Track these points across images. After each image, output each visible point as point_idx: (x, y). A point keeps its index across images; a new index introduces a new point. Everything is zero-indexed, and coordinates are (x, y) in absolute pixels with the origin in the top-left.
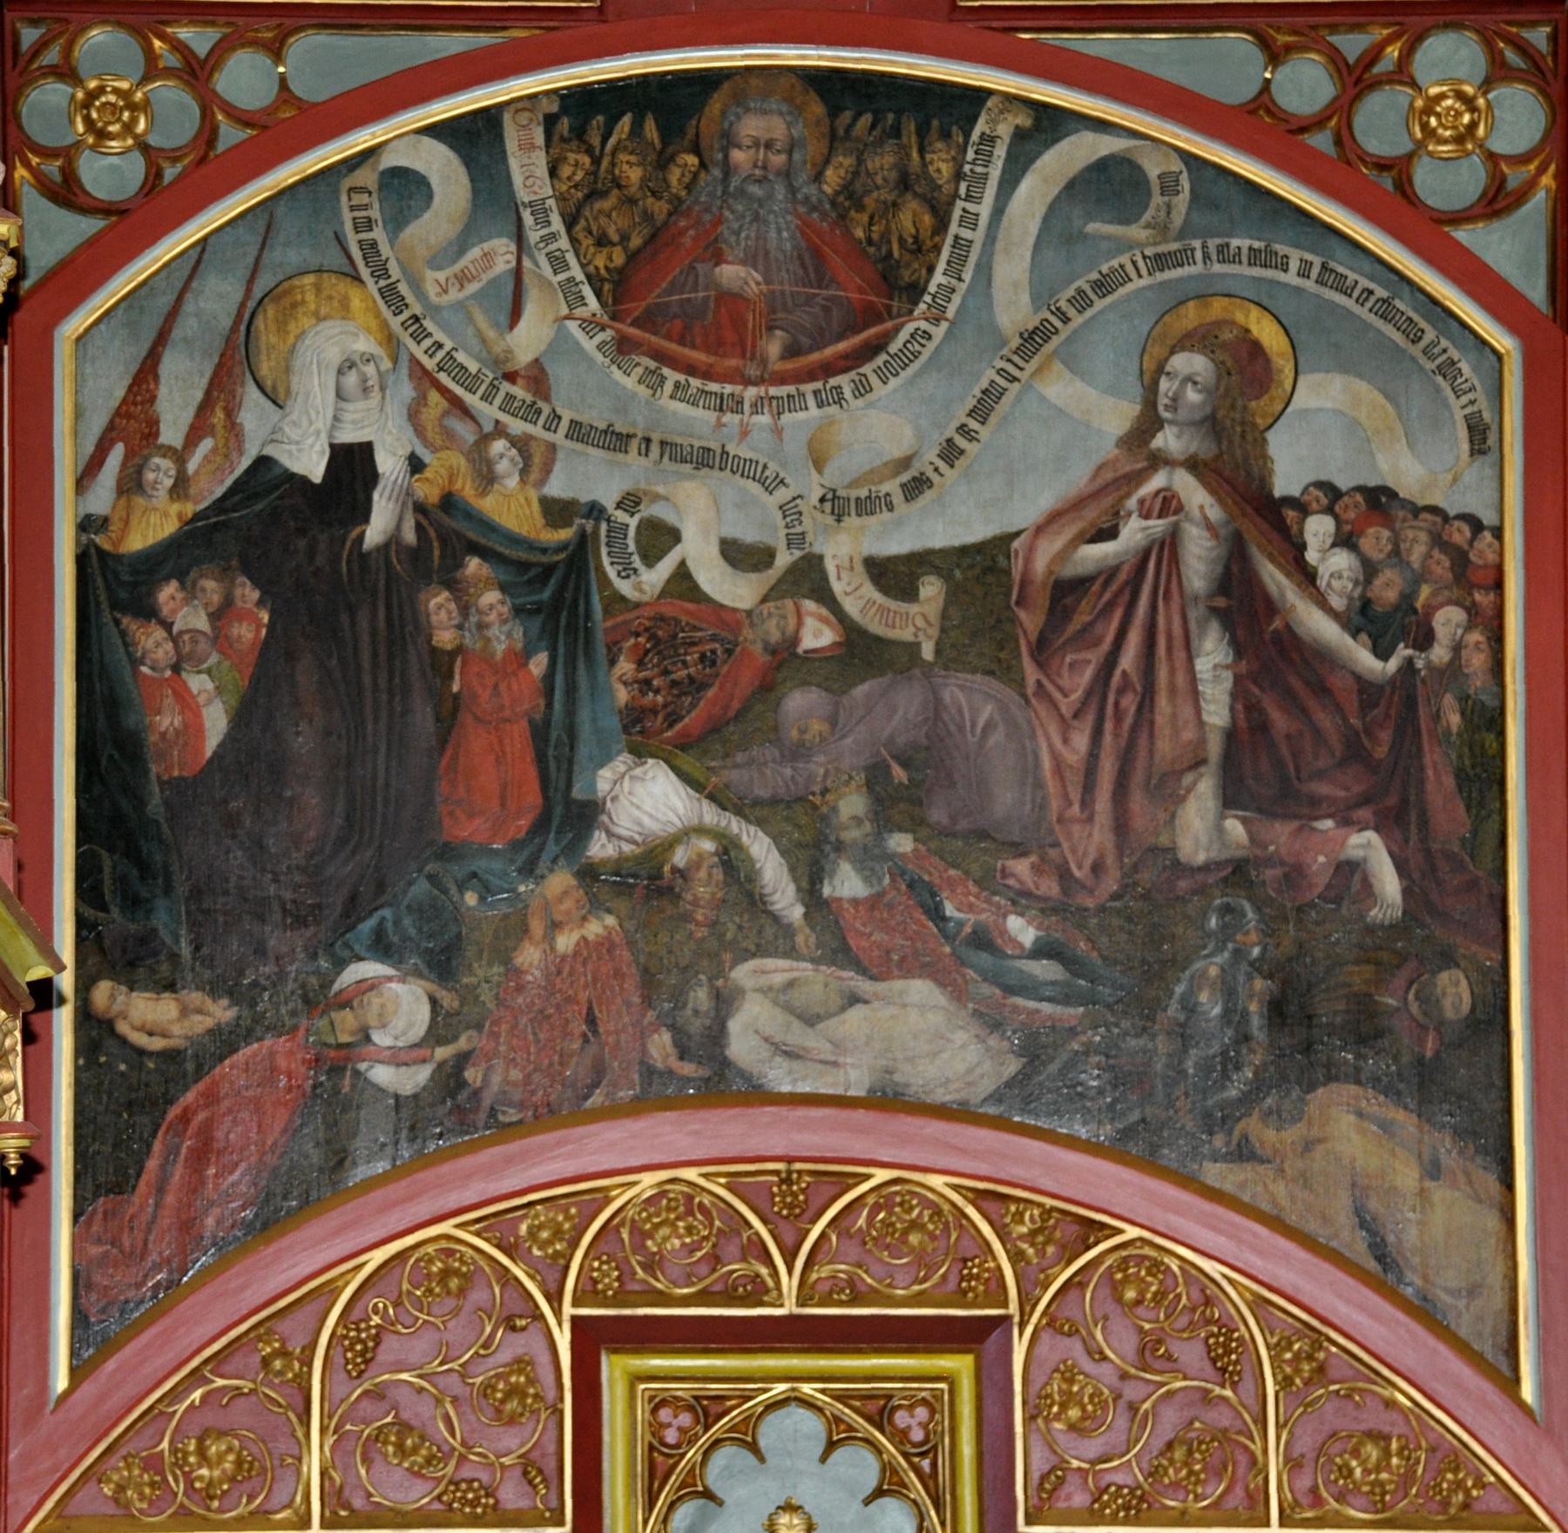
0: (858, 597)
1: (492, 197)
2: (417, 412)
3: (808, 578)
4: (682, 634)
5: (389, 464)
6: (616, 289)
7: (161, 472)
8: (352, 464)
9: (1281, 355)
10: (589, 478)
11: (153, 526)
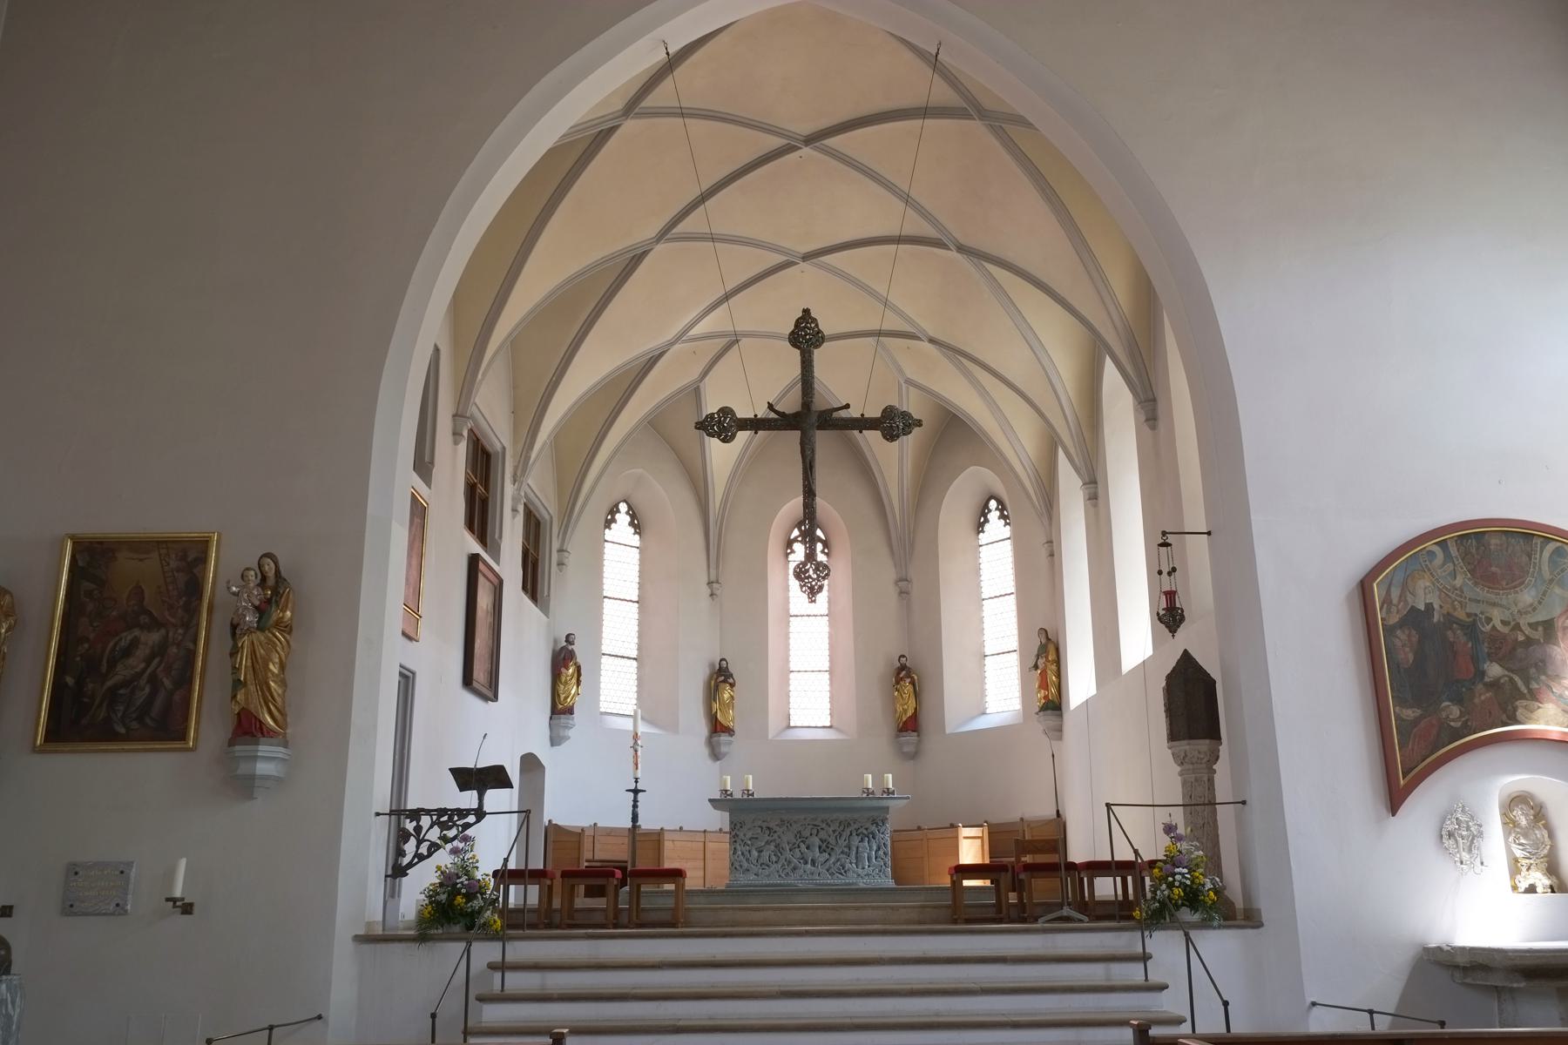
0: (1527, 631)
1: (1448, 557)
2: (1527, 803)
3: (1517, 627)
4: (1496, 639)
5: (1436, 606)
6: (1472, 572)
7: (1394, 609)
8: (1429, 607)
9: (1392, 1026)
10: (1473, 608)
11: (1394, 619)
